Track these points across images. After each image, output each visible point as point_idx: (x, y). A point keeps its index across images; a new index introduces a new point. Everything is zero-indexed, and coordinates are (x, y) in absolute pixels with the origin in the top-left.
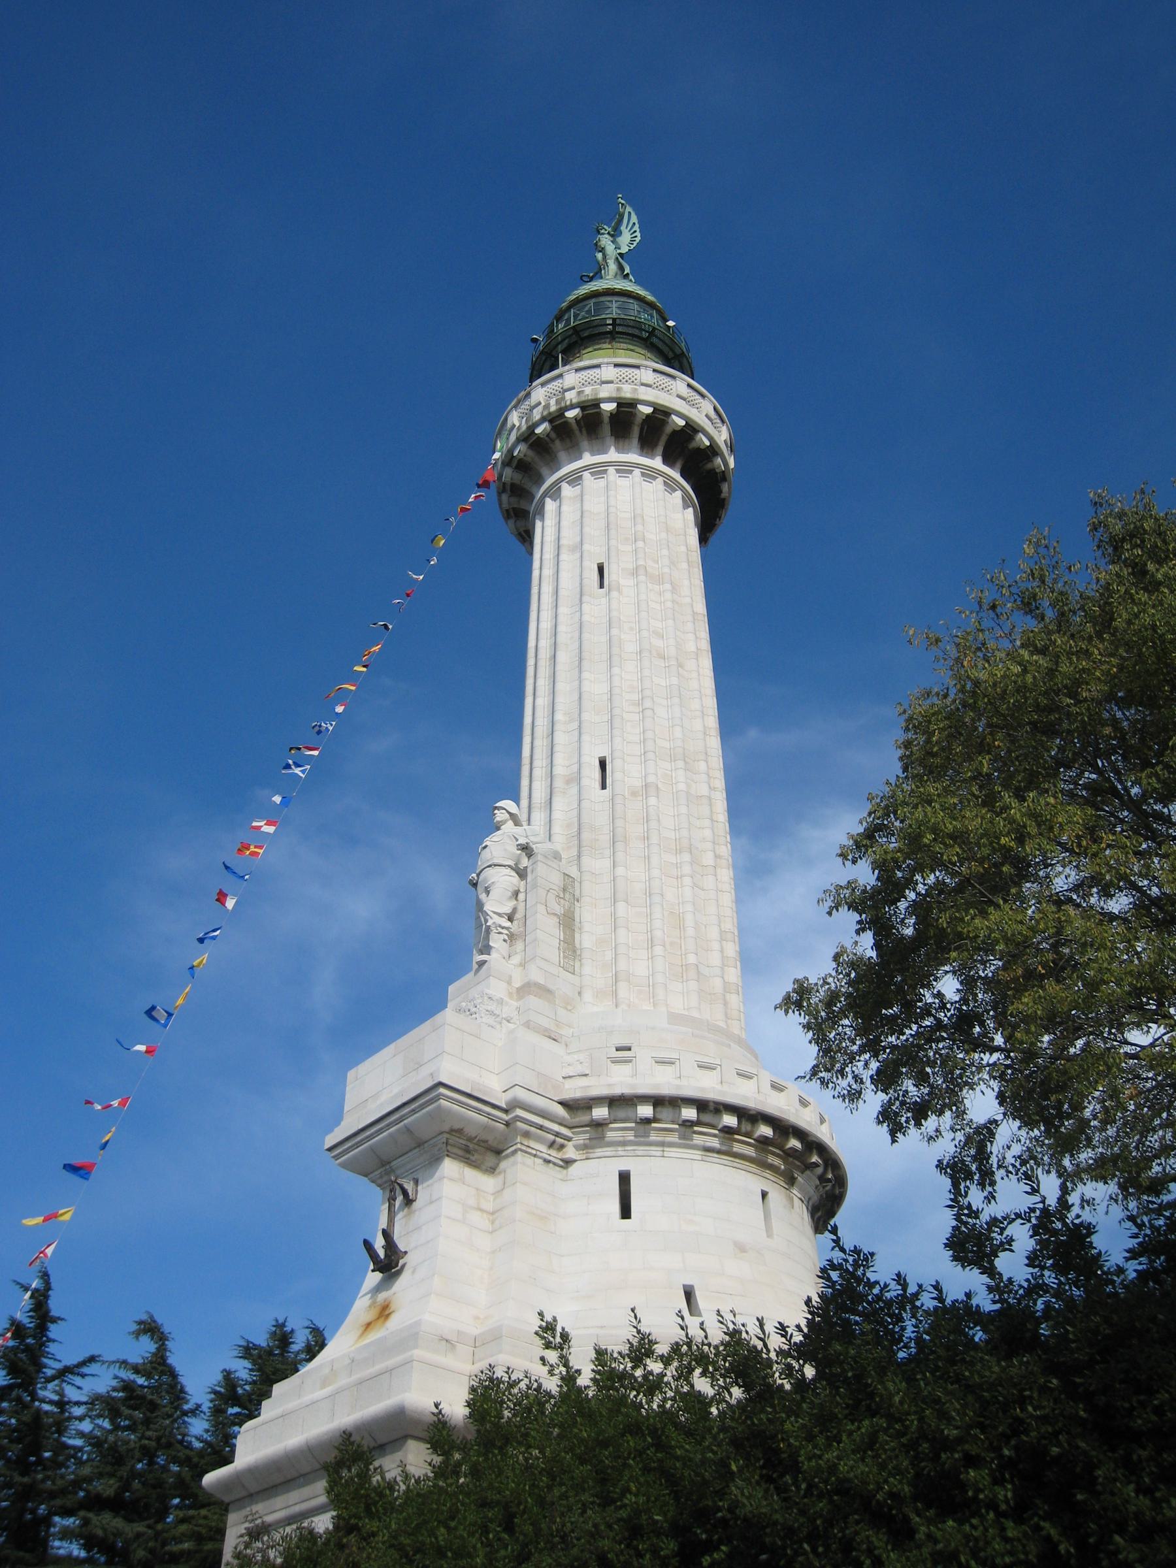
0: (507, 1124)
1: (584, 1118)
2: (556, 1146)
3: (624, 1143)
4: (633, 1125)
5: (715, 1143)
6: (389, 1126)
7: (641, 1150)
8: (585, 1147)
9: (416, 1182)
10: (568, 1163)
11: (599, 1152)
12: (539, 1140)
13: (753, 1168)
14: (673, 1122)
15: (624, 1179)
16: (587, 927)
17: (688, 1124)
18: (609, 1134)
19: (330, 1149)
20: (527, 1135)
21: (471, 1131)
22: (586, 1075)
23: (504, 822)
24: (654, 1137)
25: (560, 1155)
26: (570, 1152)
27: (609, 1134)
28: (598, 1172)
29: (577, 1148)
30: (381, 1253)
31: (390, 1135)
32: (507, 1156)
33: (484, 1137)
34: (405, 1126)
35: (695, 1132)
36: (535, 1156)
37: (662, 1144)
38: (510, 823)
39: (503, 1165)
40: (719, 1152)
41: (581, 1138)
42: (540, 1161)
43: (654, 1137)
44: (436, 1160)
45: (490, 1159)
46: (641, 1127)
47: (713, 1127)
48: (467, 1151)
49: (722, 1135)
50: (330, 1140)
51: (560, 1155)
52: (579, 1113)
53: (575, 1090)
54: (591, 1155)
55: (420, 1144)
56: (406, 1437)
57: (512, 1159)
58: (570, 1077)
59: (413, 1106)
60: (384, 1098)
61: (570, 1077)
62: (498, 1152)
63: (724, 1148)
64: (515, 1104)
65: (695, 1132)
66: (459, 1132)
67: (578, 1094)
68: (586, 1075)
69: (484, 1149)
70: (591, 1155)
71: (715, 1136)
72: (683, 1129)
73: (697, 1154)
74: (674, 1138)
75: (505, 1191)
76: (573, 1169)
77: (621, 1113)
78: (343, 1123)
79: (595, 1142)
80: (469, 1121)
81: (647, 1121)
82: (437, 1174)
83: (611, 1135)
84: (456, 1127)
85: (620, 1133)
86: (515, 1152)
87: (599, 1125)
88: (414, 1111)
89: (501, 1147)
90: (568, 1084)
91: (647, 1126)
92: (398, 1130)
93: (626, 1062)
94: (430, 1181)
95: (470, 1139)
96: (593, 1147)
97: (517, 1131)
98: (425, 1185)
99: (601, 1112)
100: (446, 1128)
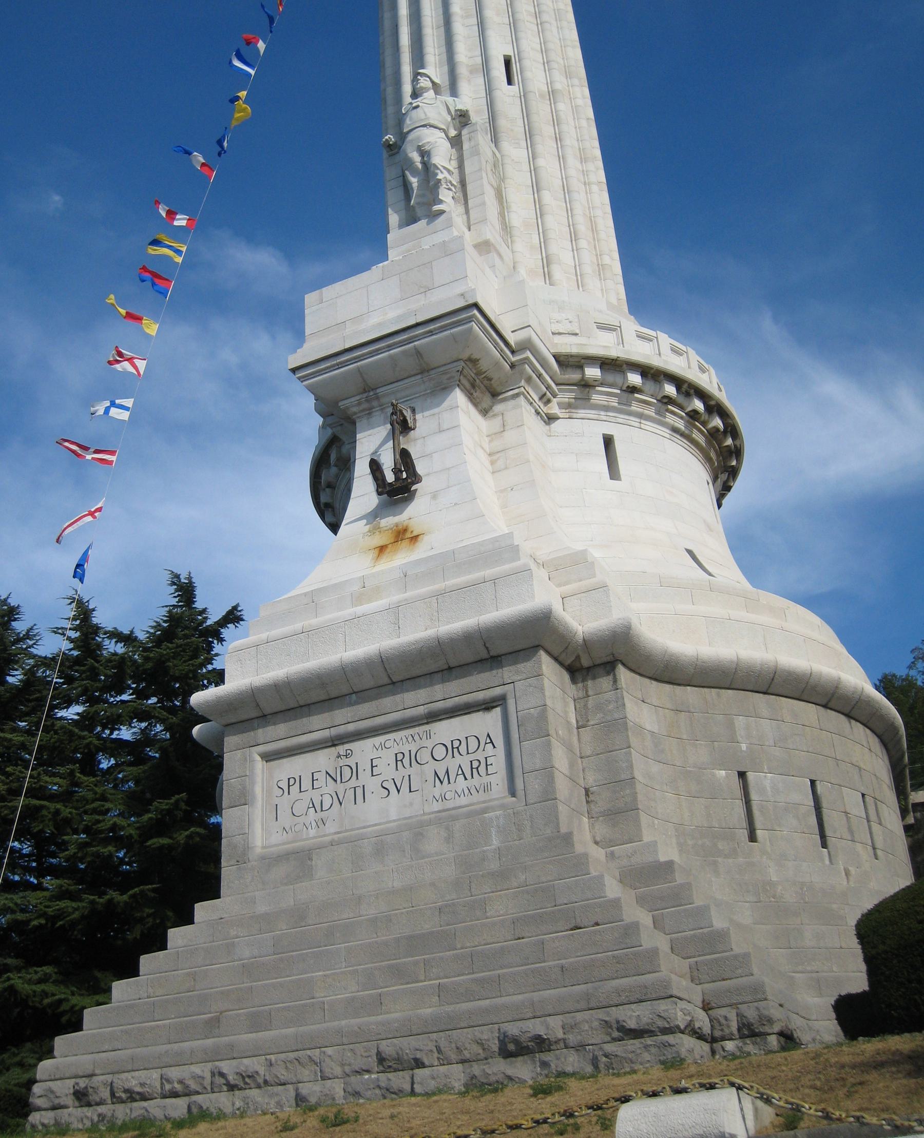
0: (512, 366)
1: (575, 376)
2: (545, 399)
3: (607, 408)
4: (619, 391)
5: (680, 424)
6: (390, 347)
7: (622, 417)
8: (569, 406)
9: (414, 411)
10: (550, 419)
11: (582, 413)
12: (536, 388)
13: (700, 456)
14: (652, 396)
15: (608, 442)
16: (514, 207)
17: (667, 400)
18: (595, 397)
19: (294, 370)
20: (529, 380)
21: (484, 365)
22: (576, 334)
23: (426, 90)
24: (635, 407)
25: (545, 409)
26: (554, 409)
27: (595, 397)
28: (584, 430)
29: (560, 405)
30: (390, 477)
31: (390, 357)
32: (505, 400)
33: (490, 374)
34: (415, 347)
35: (668, 410)
36: (531, 404)
37: (641, 416)
38: (432, 92)
39: (498, 408)
40: (682, 435)
41: (566, 396)
42: (533, 411)
43: (635, 407)
44: (442, 390)
45: (487, 400)
46: (626, 395)
47: (682, 408)
48: (473, 386)
49: (687, 418)
50: (296, 360)
51: (545, 409)
52: (569, 370)
53: (570, 346)
54: (575, 415)
55: (424, 371)
56: (537, 647)
57: (511, 403)
58: (560, 334)
59: (432, 327)
60: (374, 320)
61: (560, 334)
62: (494, 394)
63: (687, 432)
64: (527, 345)
65: (668, 410)
66: (473, 361)
67: (574, 350)
68: (576, 334)
69: (487, 390)
70: (575, 415)
71: (681, 418)
72: (660, 404)
73: (666, 432)
74: (651, 412)
75: (505, 433)
76: (556, 425)
77: (610, 378)
78: (305, 346)
79: (579, 402)
80: (487, 352)
81: (633, 390)
82: (446, 404)
83: (596, 398)
84: (475, 356)
85: (604, 398)
86: (517, 396)
87: (586, 385)
88: (431, 333)
89: (499, 389)
90: (557, 339)
91: (631, 395)
92: (403, 352)
93: (610, 329)
94: (436, 410)
95: (478, 374)
96: (576, 408)
97: (522, 372)
98: (427, 413)
99: (592, 372)
100: (465, 356)
